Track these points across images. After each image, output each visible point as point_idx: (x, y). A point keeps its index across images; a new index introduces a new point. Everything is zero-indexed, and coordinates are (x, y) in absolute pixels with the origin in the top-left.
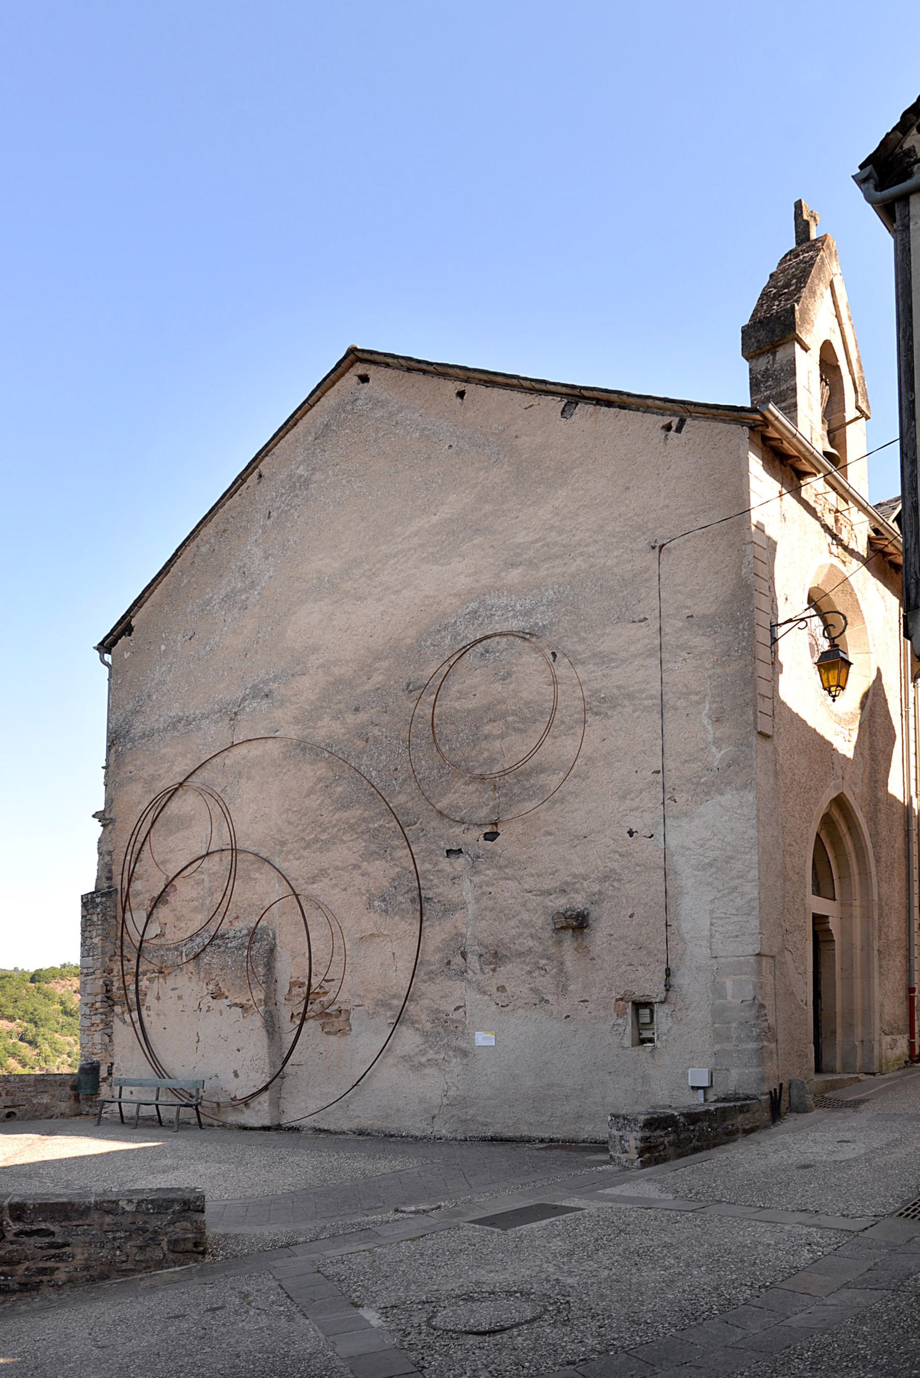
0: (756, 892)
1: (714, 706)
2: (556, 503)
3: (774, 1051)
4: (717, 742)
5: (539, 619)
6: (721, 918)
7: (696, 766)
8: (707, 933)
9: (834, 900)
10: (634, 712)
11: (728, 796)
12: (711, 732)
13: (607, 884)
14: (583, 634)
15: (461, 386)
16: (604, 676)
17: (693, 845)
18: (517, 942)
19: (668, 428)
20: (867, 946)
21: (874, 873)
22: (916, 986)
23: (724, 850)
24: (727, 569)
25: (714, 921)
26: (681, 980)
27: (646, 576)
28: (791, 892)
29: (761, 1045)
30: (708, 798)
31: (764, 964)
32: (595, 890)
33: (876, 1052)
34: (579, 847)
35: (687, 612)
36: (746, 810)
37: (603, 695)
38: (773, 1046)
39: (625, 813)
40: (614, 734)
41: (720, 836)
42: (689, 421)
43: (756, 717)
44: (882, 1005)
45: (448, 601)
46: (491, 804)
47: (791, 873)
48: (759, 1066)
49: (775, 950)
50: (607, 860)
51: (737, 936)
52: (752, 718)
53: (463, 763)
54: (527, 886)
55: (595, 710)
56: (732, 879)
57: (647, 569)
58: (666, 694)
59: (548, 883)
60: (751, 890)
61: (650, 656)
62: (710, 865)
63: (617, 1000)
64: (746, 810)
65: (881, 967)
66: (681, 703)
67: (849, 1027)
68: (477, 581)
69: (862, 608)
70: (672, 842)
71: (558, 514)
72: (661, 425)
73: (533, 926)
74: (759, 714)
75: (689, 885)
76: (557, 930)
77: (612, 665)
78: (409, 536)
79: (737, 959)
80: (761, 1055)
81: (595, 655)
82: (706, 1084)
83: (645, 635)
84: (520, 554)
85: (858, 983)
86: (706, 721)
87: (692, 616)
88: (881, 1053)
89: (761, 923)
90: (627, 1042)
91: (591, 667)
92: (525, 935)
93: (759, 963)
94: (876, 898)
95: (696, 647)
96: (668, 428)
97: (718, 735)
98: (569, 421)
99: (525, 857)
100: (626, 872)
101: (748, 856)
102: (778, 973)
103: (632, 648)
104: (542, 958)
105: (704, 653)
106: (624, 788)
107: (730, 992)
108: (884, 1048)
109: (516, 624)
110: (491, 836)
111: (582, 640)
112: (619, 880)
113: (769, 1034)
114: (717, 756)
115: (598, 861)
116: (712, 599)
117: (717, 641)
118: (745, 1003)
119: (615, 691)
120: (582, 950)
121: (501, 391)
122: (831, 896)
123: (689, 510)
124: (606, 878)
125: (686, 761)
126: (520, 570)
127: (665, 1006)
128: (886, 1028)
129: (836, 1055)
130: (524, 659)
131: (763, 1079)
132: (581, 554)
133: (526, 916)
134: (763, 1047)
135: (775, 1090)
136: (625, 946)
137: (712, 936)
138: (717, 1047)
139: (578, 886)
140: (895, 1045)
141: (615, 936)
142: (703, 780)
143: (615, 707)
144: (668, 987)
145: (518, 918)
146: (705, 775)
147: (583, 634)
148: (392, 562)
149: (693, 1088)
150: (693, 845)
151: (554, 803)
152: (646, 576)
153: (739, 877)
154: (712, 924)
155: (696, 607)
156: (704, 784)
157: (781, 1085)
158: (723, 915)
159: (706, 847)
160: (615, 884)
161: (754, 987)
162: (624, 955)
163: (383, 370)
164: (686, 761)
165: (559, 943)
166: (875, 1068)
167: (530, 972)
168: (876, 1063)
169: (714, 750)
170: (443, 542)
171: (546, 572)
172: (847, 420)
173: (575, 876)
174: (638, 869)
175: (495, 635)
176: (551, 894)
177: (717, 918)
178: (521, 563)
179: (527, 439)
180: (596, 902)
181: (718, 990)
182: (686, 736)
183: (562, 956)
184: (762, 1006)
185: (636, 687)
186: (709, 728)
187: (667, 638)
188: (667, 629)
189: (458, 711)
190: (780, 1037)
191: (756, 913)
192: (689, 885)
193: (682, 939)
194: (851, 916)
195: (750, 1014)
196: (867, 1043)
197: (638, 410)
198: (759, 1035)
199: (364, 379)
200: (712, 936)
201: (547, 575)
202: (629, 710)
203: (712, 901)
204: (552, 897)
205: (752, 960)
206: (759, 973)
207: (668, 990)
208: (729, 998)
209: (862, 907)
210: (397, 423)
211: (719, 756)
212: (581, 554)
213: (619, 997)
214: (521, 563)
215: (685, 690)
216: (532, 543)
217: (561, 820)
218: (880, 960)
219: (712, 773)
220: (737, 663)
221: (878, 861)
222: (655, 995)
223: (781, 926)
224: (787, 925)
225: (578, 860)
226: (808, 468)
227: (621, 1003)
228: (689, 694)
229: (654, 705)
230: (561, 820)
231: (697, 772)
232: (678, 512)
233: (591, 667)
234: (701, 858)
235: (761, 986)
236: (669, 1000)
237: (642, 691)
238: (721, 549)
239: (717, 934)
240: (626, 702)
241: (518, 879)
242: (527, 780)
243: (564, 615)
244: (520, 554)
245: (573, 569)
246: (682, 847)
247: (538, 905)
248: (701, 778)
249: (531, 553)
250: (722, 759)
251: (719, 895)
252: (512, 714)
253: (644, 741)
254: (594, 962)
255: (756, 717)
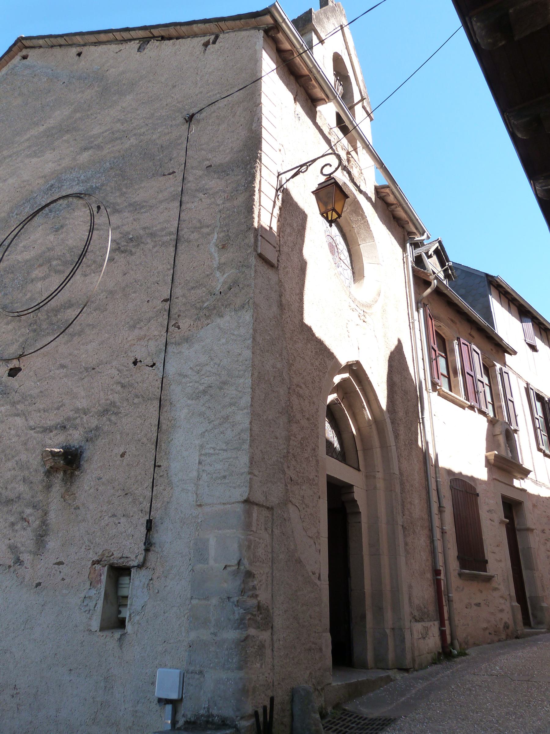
0: (248, 422)
1: (222, 234)
2: (124, 105)
3: (267, 644)
4: (221, 267)
5: (94, 183)
6: (210, 455)
7: (200, 292)
8: (195, 474)
9: (359, 470)
10: (154, 247)
11: (227, 318)
12: (217, 258)
13: (105, 418)
14: (124, 190)
15: (79, 49)
16: (134, 220)
17: (190, 372)
18: (9, 487)
19: (206, 45)
20: (392, 522)
21: (394, 448)
22: (441, 568)
23: (219, 375)
24: (241, 128)
25: (203, 458)
26: (164, 536)
27: (179, 141)
28: (299, 438)
29: (245, 634)
30: (209, 321)
31: (255, 515)
32: (93, 426)
33: (408, 644)
34: (86, 380)
35: (207, 163)
36: (242, 331)
37: (131, 236)
38: (265, 636)
39: (132, 342)
40: (135, 268)
41: (217, 361)
42: (221, 36)
43: (256, 240)
44: (410, 587)
45: (37, 182)
46: (21, 340)
47: (299, 416)
48: (240, 668)
49: (274, 500)
50: (109, 393)
51: (225, 477)
52: (252, 240)
53: (10, 305)
54: (32, 423)
55: (122, 248)
56: (224, 407)
57: (181, 137)
58: (182, 230)
59: (52, 419)
60: (242, 419)
61: (174, 200)
62: (205, 392)
63: (94, 563)
64: (242, 331)
65: (406, 544)
66: (195, 235)
67: (379, 610)
68: (60, 165)
69: (371, 229)
70: (171, 369)
71: (124, 111)
72: (203, 42)
73: (28, 468)
74: (260, 238)
75: (182, 417)
76: (49, 473)
77: (142, 211)
78: (23, 142)
79: (222, 507)
80: (246, 651)
81: (130, 205)
82: (174, 696)
83: (172, 185)
84: (93, 142)
85: (385, 560)
86: (213, 249)
87: (211, 166)
88: (413, 644)
89: (252, 461)
90: (95, 624)
91: (126, 214)
92: (19, 478)
93: (248, 514)
94: (397, 472)
95: (211, 189)
96: (206, 45)
97: (223, 261)
98: (142, 54)
99: (37, 391)
100: (125, 405)
101: (242, 380)
102: (276, 532)
103: (160, 196)
104: (27, 506)
105: (217, 192)
106: (135, 318)
107: (212, 552)
108: (416, 636)
109: (76, 189)
110: (14, 372)
111: (122, 194)
112: (116, 414)
113: (260, 616)
114: (220, 280)
115: (102, 393)
116: (228, 151)
117: (229, 181)
118: (229, 569)
119: (141, 232)
120: (68, 494)
121: (104, 46)
122: (356, 466)
123: (217, 92)
124: (106, 411)
125: (192, 288)
126: (90, 152)
127: (143, 572)
128: (416, 614)
129: (367, 648)
130: (76, 214)
131: (245, 691)
132: (135, 135)
133: (23, 457)
134: (247, 638)
135: (265, 708)
136: (112, 491)
137: (199, 478)
138: (193, 635)
139: (78, 421)
140: (427, 634)
141: (103, 480)
142: (206, 305)
143: (138, 245)
144: (148, 546)
145: (17, 458)
146: (208, 300)
147: (124, 190)
148: (7, 160)
149: (160, 700)
150: (190, 372)
151: (73, 335)
152: (179, 141)
153: (231, 405)
154: (200, 463)
155: (214, 159)
156: (207, 308)
157: (272, 699)
158: (212, 451)
159: (203, 373)
160: (113, 418)
161: (240, 546)
162: (109, 502)
163: (37, 51)
164: (192, 288)
165: (49, 487)
166: (408, 662)
167: (13, 524)
168: (409, 656)
169: (218, 274)
170: (43, 142)
171: (107, 151)
172: (355, 102)
173: (77, 410)
174: (136, 400)
175: (60, 198)
176: (51, 431)
177: (205, 455)
178: (91, 147)
179: (114, 70)
180: (91, 439)
181: (200, 552)
182: (195, 265)
183: (48, 504)
184: (249, 575)
185: (159, 227)
186: (216, 255)
187: (189, 185)
188: (190, 178)
189: (19, 262)
190: (278, 622)
191: (246, 446)
192: (182, 417)
193: (170, 483)
194: (375, 488)
195: (231, 585)
196: (399, 632)
197: (189, 37)
198: (242, 619)
199: (25, 57)
200: (199, 478)
201: (108, 153)
202: (150, 246)
203: (203, 435)
204: (52, 434)
205: (239, 508)
206: (248, 526)
207: (147, 550)
208: (211, 562)
209: (385, 480)
210: (35, 75)
211: (221, 280)
212: (135, 135)
213: (96, 558)
214: (91, 147)
215: (198, 225)
216: (103, 133)
217: (76, 352)
218: (405, 536)
219: (215, 297)
220: (243, 195)
221: (397, 437)
222: (133, 557)
223: (284, 472)
224: (291, 473)
225: (83, 394)
226: (321, 95)
227: (98, 567)
228: (201, 228)
229: (171, 240)
230: (76, 352)
231: (202, 297)
232: (208, 95)
233: (126, 214)
234: (196, 385)
235: (249, 546)
236: (148, 564)
237: (163, 229)
238: (238, 113)
239: (204, 475)
240: (149, 240)
241: (24, 415)
242: (56, 315)
243: (114, 177)
244: (93, 142)
245: (127, 146)
246: (180, 375)
247: (38, 444)
248: (204, 302)
249: (100, 140)
250: (225, 282)
251: (210, 427)
252: (57, 259)
253: (158, 273)
254: (78, 512)
255: (256, 240)
